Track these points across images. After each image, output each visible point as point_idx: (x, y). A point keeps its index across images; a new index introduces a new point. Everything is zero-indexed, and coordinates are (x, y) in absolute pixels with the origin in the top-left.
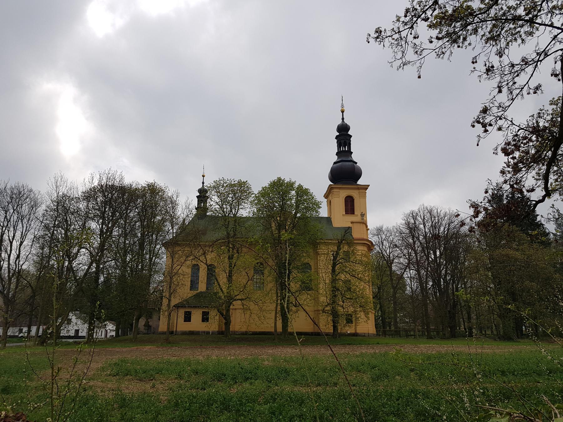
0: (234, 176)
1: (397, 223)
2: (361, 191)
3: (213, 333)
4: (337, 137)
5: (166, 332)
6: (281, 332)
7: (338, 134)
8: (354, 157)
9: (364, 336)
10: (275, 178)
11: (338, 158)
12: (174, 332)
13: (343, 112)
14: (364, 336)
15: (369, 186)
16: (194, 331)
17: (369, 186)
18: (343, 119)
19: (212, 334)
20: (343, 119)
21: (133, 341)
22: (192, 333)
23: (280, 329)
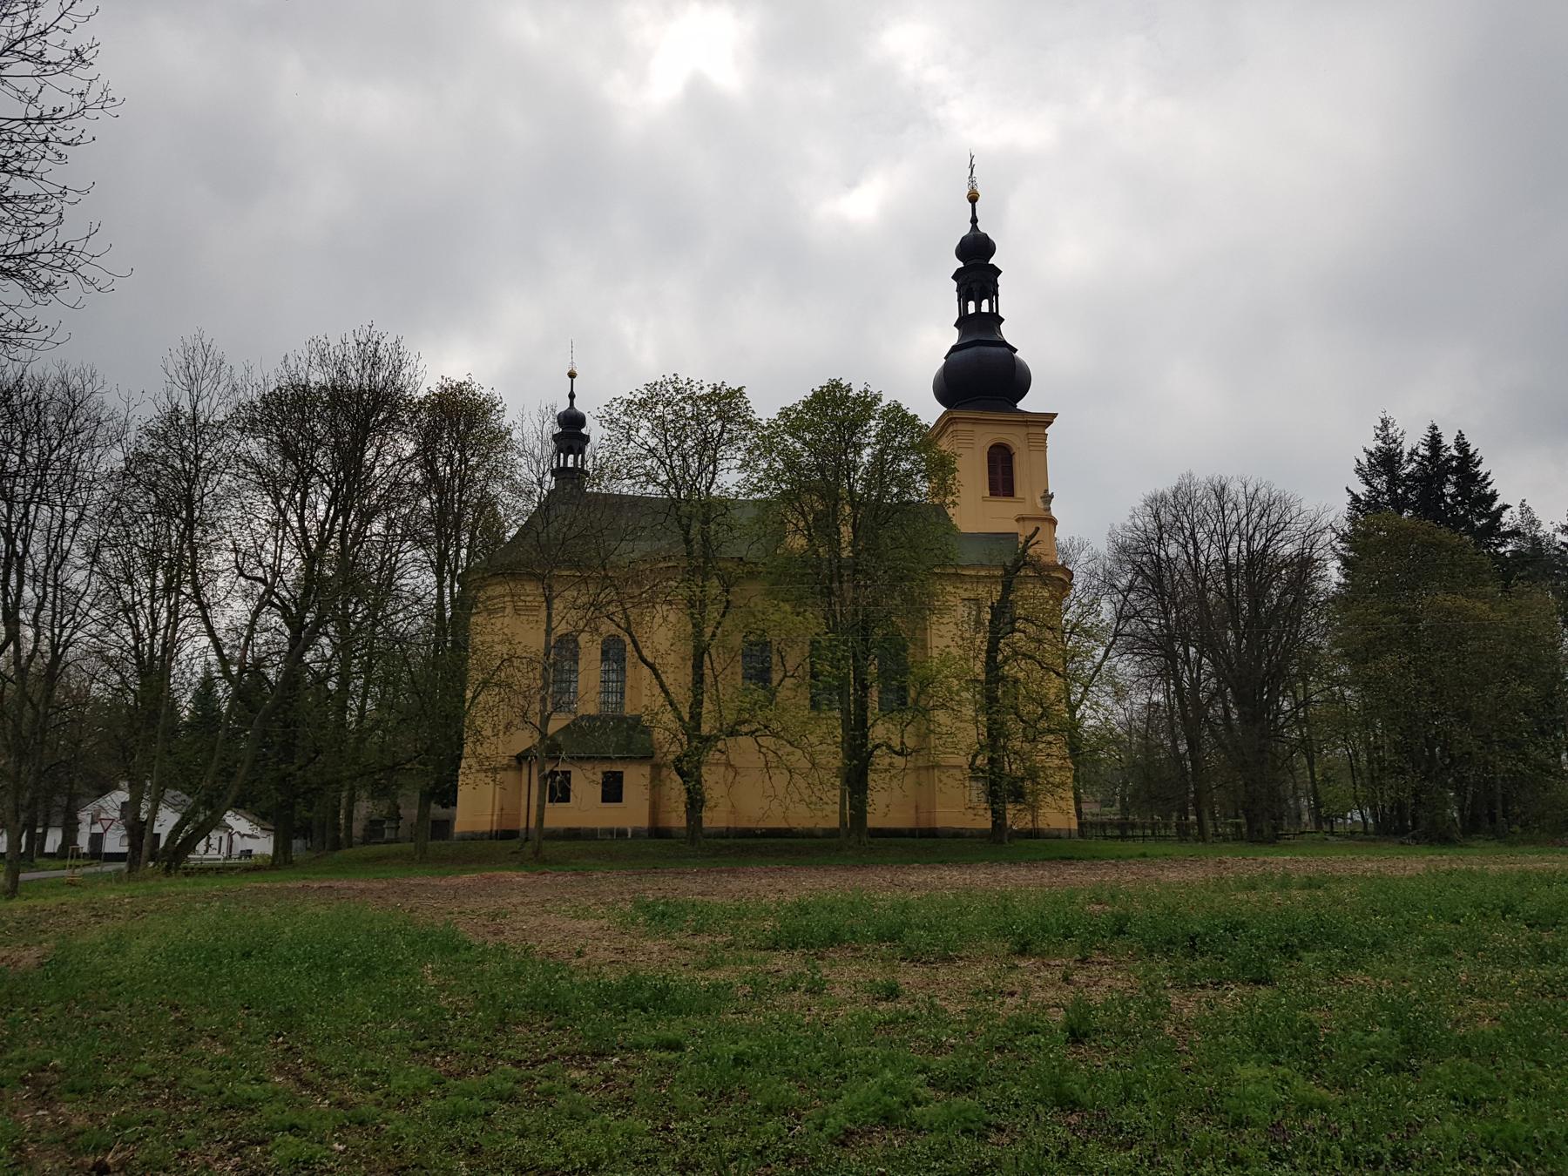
0: (703, 373)
1: (1112, 525)
2: (1032, 430)
3: (637, 833)
4: (957, 276)
5: (838, 830)
6: (987, 830)
7: (961, 265)
8: (1008, 332)
9: (1059, 837)
10: (819, 382)
11: (961, 337)
12: (522, 835)
13: (973, 199)
14: (1059, 837)
15: (1055, 415)
16: (579, 829)
17: (1055, 415)
18: (974, 220)
19: (632, 836)
20: (974, 220)
21: (417, 857)
22: (573, 834)
23: (677, 818)
